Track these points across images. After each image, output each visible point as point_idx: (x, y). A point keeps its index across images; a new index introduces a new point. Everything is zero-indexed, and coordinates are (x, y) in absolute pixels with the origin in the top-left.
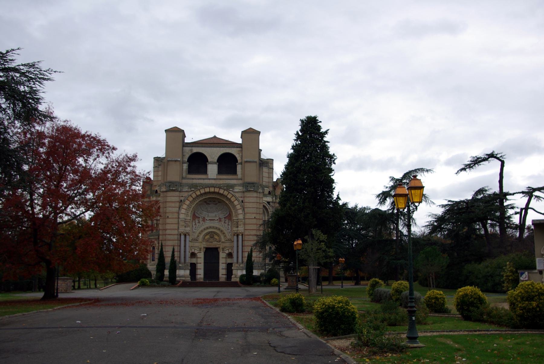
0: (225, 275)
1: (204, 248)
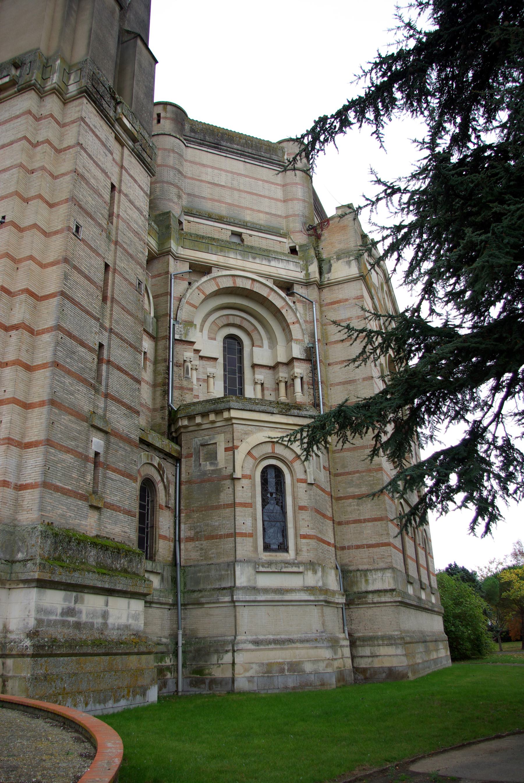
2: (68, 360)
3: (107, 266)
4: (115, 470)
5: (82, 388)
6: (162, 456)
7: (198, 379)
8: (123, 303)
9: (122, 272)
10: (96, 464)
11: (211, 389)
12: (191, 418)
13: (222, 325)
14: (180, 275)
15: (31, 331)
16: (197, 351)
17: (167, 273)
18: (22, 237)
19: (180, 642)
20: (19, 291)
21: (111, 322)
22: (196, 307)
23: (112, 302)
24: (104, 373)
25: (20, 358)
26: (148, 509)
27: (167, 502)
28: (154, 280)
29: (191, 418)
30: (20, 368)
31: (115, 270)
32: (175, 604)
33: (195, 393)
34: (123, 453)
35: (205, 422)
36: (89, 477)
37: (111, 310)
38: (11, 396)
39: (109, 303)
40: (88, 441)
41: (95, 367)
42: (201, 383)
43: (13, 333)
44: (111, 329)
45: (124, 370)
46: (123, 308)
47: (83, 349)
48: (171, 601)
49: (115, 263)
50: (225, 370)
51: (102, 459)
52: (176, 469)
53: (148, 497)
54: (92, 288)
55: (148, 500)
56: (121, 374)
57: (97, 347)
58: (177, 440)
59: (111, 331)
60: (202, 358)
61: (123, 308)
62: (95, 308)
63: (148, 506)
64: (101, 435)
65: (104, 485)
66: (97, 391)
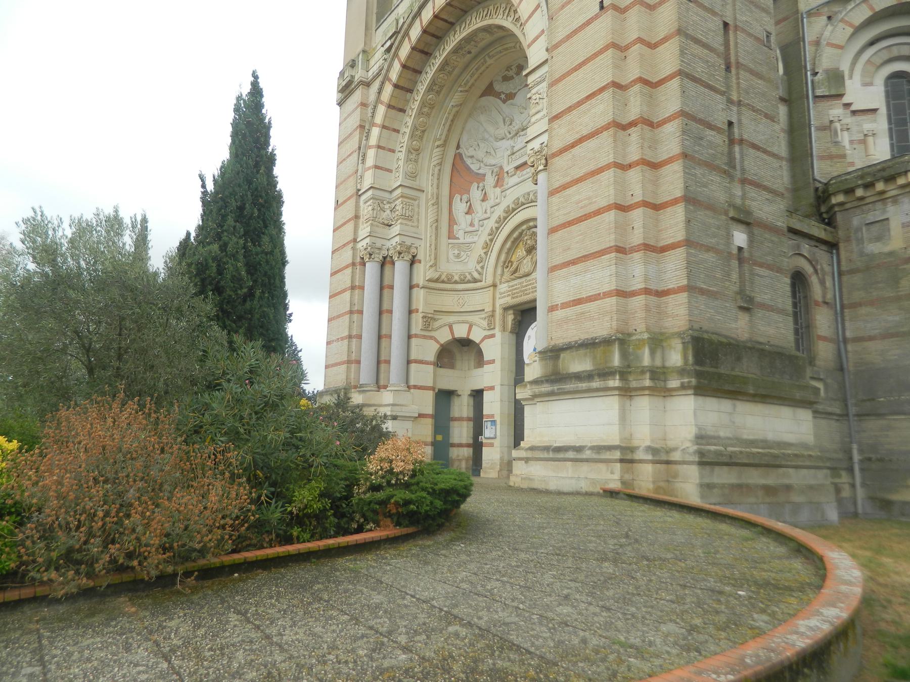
0: (468, 446)
1: (506, 309)
2: (697, 148)
3: (726, 25)
4: (761, 265)
5: (716, 178)
6: (813, 243)
7: (851, 142)
8: (752, 66)
9: (746, 28)
10: (741, 260)
11: (872, 150)
12: (850, 191)
13: (881, 61)
14: (815, 11)
15: (651, 124)
16: (847, 105)
17: (797, 11)
18: (625, 19)
19: (856, 457)
20: (631, 82)
21: (739, 93)
22: (841, 47)
23: (737, 68)
24: (737, 156)
25: (644, 157)
26: (800, 307)
27: (824, 296)
28: (778, 26)
29: (850, 191)
30: (645, 168)
31: (736, 28)
32: (845, 415)
33: (849, 160)
34: (770, 245)
35: (868, 194)
36: (735, 276)
37: (738, 78)
38: (641, 199)
39: (733, 71)
40: (729, 237)
41: (726, 150)
42: (855, 146)
43: (632, 130)
44: (740, 101)
45: (761, 148)
46: (752, 72)
47: (713, 133)
48: (838, 411)
49: (735, 19)
50: (890, 122)
51: (746, 254)
52: (832, 257)
53: (799, 292)
54: (713, 58)
55: (799, 297)
56: (759, 153)
57: (726, 127)
58: (830, 222)
59: (739, 103)
60: (854, 113)
61: (752, 72)
62: (719, 80)
63: (800, 303)
64: (742, 227)
65: (752, 283)
66: (731, 177)
